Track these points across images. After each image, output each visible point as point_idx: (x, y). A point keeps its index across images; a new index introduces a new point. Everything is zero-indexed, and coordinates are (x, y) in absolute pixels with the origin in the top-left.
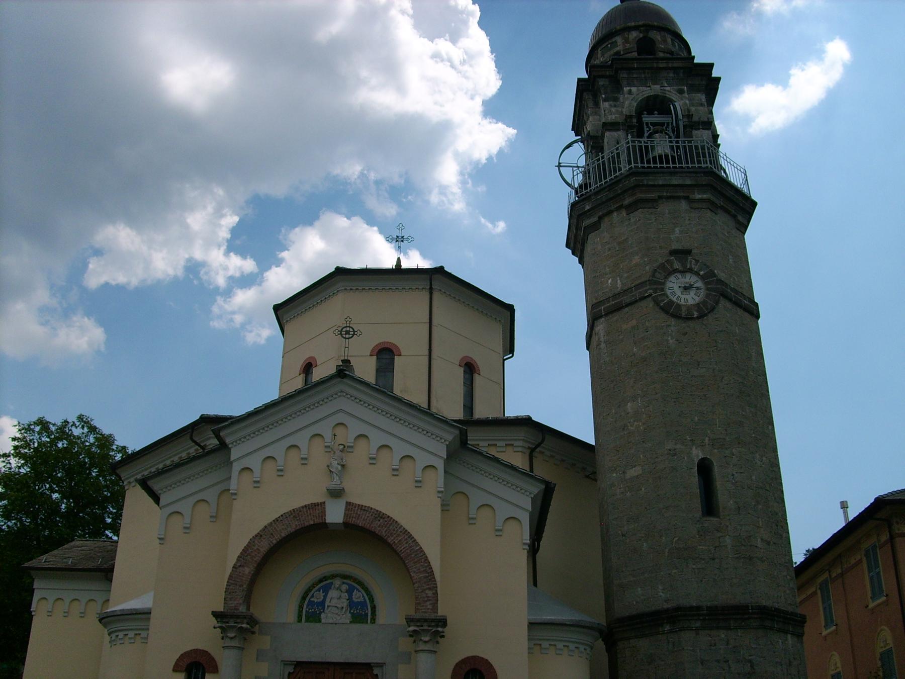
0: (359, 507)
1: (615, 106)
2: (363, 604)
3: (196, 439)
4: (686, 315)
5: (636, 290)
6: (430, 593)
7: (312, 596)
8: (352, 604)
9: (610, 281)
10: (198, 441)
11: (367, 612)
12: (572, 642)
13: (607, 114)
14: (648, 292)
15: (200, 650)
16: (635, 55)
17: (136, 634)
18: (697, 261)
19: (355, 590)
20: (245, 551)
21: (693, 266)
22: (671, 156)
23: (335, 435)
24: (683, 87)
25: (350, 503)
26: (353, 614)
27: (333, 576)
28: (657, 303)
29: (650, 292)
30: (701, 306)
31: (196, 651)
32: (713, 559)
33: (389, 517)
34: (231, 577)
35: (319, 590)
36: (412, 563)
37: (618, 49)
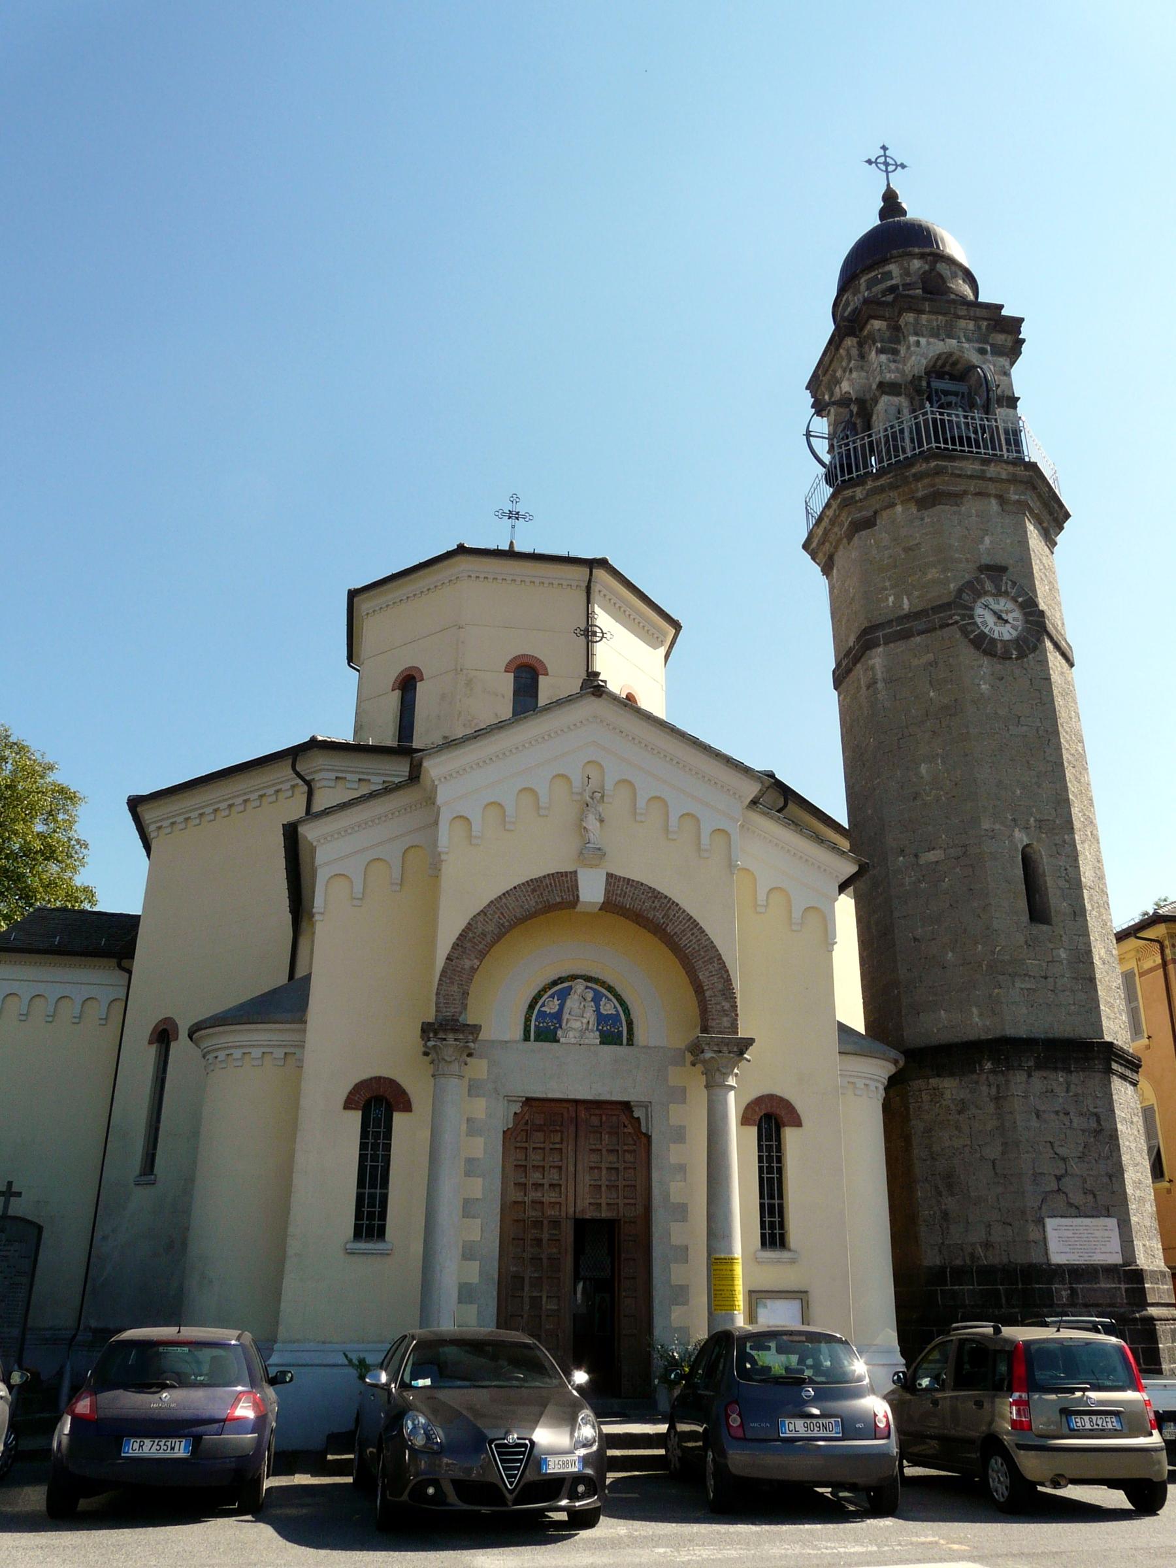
0: (624, 881)
1: (895, 361)
2: (615, 1018)
3: (298, 769)
4: (1001, 653)
5: (934, 614)
6: (727, 1006)
7: (543, 1005)
8: (601, 1018)
9: (891, 599)
10: (302, 773)
11: (621, 1029)
12: (860, 1077)
13: (885, 371)
14: (954, 618)
15: (384, 1078)
16: (919, 292)
17: (244, 1053)
18: (1014, 583)
19: (604, 999)
20: (462, 936)
21: (1009, 590)
22: (966, 437)
23: (589, 778)
24: (985, 346)
25: (612, 874)
26: (601, 1031)
27: (573, 978)
28: (965, 632)
29: (957, 618)
30: (1021, 643)
31: (378, 1080)
32: (1046, 978)
33: (666, 897)
34: (444, 973)
35: (552, 996)
36: (700, 962)
37: (893, 282)
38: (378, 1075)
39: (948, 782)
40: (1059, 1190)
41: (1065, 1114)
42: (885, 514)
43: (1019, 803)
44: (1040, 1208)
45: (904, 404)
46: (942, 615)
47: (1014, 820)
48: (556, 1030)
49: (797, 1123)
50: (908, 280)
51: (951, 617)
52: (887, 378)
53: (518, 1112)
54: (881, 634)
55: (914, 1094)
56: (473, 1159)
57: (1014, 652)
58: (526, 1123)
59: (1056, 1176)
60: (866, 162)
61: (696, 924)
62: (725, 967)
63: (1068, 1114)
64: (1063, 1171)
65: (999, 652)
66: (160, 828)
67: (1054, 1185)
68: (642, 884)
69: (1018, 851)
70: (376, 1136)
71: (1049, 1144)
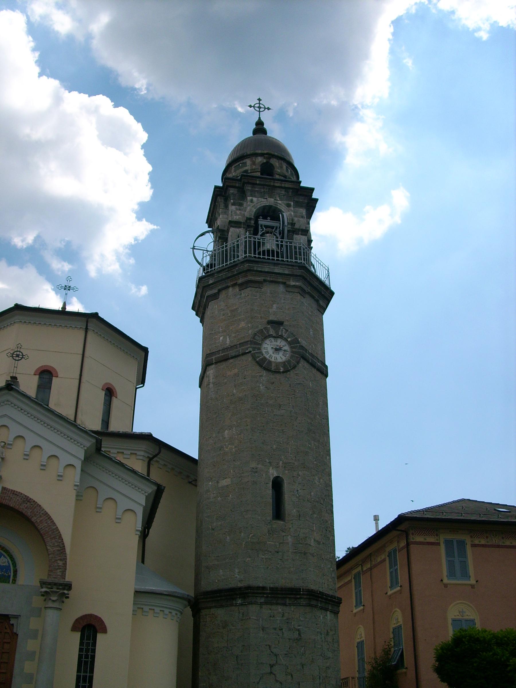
1: (240, 210)
5: (240, 347)
6: (61, 563)
9: (221, 338)
11: (10, 574)
16: (258, 174)
18: (287, 331)
22: (276, 251)
28: (254, 357)
29: (251, 349)
33: (34, 501)
40: (271, 673)
41: (280, 629)
43: (274, 453)
44: (258, 683)
45: (242, 233)
46: (243, 348)
47: (270, 462)
49: (104, 630)
50: (254, 167)
52: (234, 218)
54: (214, 358)
57: (282, 369)
59: (270, 665)
60: (270, 109)
61: (50, 518)
62: (63, 541)
63: (282, 629)
64: (275, 662)
65: (273, 368)
67: (268, 670)
68: (22, 494)
69: (270, 480)
71: (268, 647)
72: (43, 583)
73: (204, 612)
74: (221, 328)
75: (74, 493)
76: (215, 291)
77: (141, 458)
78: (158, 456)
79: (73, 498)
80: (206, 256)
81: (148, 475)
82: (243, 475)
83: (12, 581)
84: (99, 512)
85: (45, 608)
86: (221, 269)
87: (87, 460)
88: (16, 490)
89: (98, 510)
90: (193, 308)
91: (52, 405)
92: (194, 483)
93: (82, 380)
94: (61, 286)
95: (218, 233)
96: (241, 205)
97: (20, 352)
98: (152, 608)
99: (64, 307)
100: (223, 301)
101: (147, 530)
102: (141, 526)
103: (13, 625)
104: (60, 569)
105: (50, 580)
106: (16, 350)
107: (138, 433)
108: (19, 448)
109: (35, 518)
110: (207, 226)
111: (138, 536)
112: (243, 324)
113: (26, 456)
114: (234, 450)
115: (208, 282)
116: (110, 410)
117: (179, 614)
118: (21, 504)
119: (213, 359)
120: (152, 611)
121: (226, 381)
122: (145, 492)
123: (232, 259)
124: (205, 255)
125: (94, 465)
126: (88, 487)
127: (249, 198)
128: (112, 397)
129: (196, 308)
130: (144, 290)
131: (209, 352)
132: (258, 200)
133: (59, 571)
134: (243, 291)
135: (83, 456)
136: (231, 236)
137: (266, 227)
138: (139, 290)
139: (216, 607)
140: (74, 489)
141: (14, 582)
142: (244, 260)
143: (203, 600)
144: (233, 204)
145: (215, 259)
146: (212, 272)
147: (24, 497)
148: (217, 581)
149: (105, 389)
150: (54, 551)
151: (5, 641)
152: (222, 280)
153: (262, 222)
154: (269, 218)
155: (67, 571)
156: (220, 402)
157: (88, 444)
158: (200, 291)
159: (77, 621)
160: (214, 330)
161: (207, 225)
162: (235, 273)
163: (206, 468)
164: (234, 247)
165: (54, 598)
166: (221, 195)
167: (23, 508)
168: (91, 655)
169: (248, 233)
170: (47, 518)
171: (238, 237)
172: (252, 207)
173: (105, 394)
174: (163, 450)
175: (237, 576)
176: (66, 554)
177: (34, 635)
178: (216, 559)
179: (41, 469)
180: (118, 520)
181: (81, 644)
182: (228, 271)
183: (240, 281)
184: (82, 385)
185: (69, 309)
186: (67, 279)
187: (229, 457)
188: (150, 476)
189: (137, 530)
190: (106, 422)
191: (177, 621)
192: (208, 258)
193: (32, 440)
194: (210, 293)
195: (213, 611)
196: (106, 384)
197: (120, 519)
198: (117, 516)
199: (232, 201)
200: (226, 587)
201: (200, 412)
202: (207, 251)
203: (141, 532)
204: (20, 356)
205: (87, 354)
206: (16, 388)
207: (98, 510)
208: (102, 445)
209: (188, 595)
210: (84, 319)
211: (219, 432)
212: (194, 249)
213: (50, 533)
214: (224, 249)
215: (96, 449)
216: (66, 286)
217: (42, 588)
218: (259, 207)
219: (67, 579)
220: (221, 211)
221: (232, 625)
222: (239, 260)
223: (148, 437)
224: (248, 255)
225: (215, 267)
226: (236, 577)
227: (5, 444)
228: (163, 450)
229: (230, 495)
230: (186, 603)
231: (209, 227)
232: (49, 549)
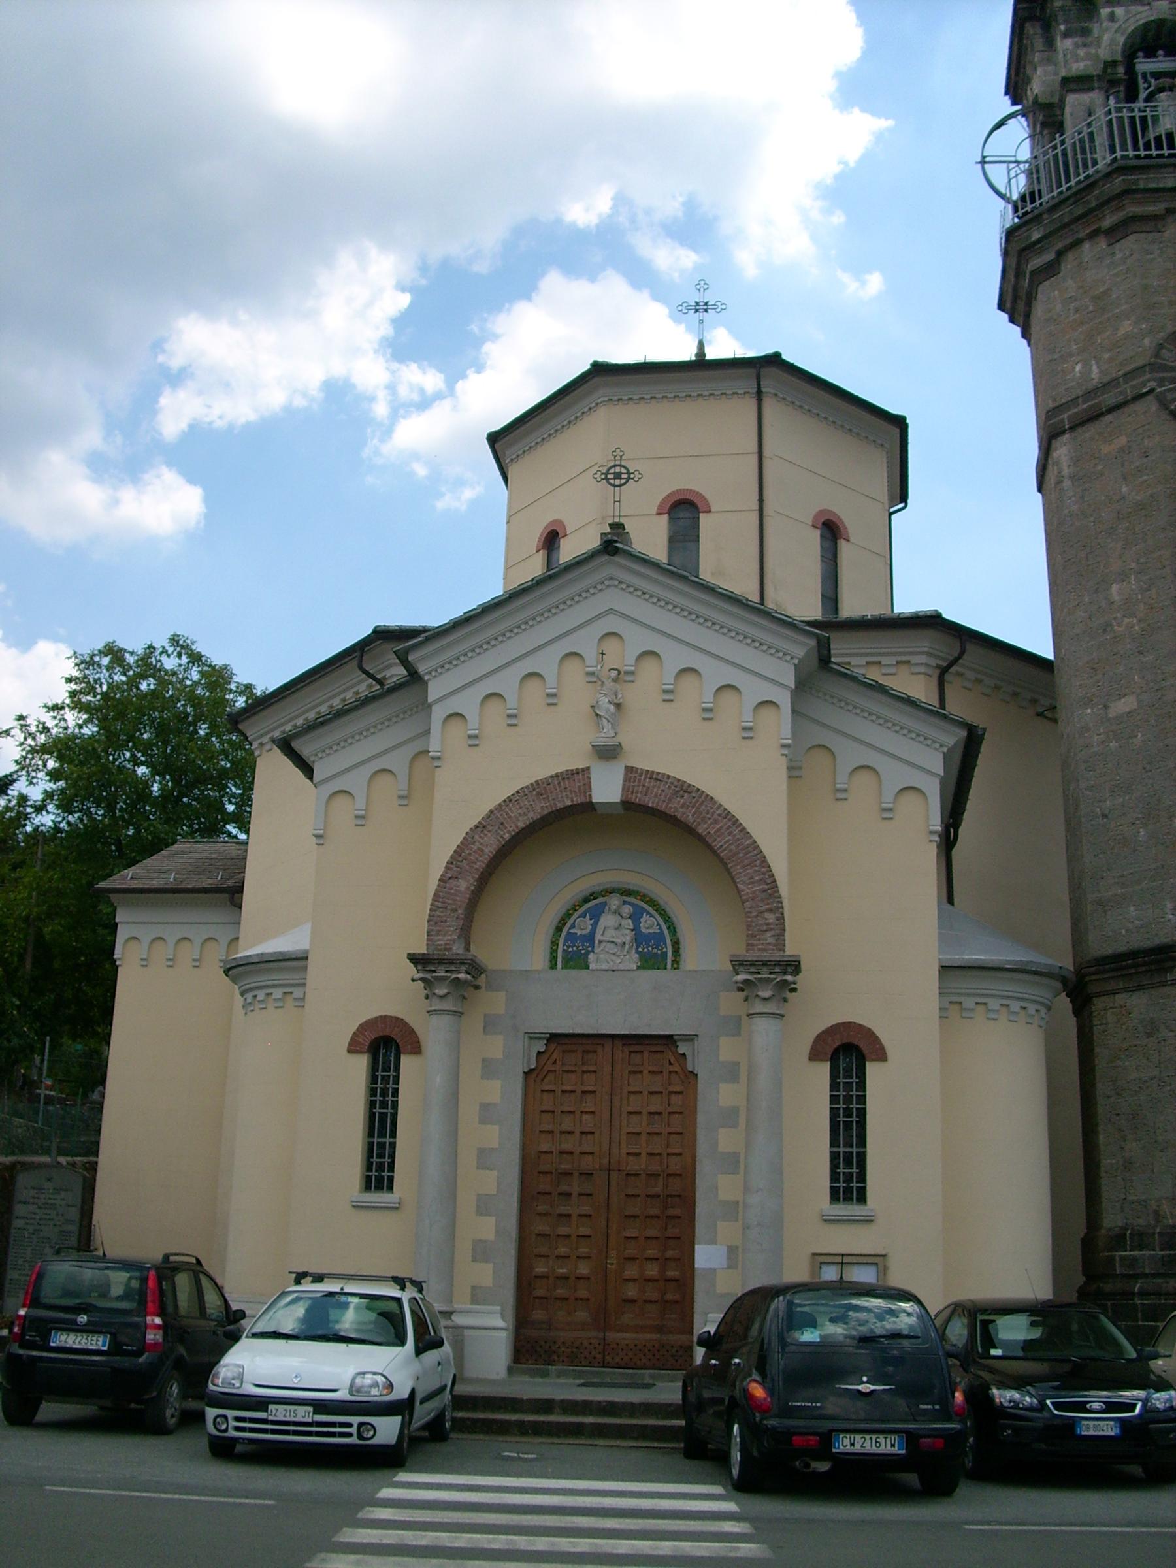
1: (1085, 45)
2: (659, 938)
6: (771, 918)
7: (573, 926)
8: (639, 938)
9: (1078, 368)
17: (285, 993)
20: (458, 852)
23: (602, 654)
29: (1152, 384)
31: (383, 1019)
33: (698, 790)
34: (436, 897)
35: (583, 915)
38: (383, 1014)
39: (1142, 605)
42: (1070, 256)
46: (1134, 382)
48: (588, 953)
49: (881, 1055)
51: (1144, 384)
53: (542, 1050)
54: (1066, 416)
55: (1099, 1014)
56: (489, 1105)
58: (555, 1062)
61: (736, 822)
66: (262, 745)
68: (669, 776)
70: (385, 1080)
72: (738, 964)
73: (1099, 1003)
74: (1073, 343)
75: (783, 763)
76: (1049, 256)
77: (923, 669)
78: (960, 661)
79: (783, 773)
80: (1016, 176)
81: (942, 705)
82: (1164, 684)
83: (672, 965)
84: (841, 799)
85: (749, 1015)
86: (1057, 200)
87: (803, 687)
88: (656, 770)
89: (840, 794)
90: (1001, 306)
91: (706, 573)
92: (1049, 714)
93: (767, 511)
94: (685, 305)
95: (1037, 112)
96: (1086, 32)
97: (620, 466)
98: (1005, 1002)
99: (701, 353)
100: (1072, 278)
101: (952, 830)
102: (939, 823)
103: (684, 1055)
104: (771, 929)
105: (752, 956)
106: (613, 464)
107: (909, 615)
108: (650, 678)
109: (705, 826)
110: (1009, 102)
111: (935, 845)
112: (1126, 327)
113: (669, 695)
114: (1137, 628)
115: (1029, 237)
116: (836, 572)
117: (1043, 1011)
118: (670, 800)
119: (1063, 419)
120: (956, 1007)
121: (1100, 467)
122: (941, 746)
123: (1081, 171)
124: (1012, 174)
125: (818, 697)
126: (814, 747)
127: (1105, 12)
128: (838, 541)
129: (1008, 305)
130: (875, 282)
131: (1051, 405)
132: (1127, 12)
133: (769, 934)
134: (1117, 246)
135: (793, 678)
136: (1071, 115)
137: (1157, 75)
138: (863, 283)
139: (1125, 990)
140: (783, 755)
141: (675, 966)
142: (1110, 169)
143: (1093, 977)
144: (1066, 35)
145: (1038, 179)
146: (1036, 212)
147: (676, 783)
148: (1124, 932)
149: (820, 525)
150: (754, 893)
151: (671, 1089)
152: (1065, 226)
153: (1144, 65)
154: (1161, 52)
155: (787, 934)
156: (1092, 519)
157: (800, 652)
158: (1013, 261)
159: (821, 1038)
160: (1057, 351)
161: (1007, 100)
162: (1094, 204)
163: (1076, 676)
164: (1081, 141)
165: (766, 994)
166: (1031, 18)
167: (675, 807)
168: (857, 1109)
169: (1112, 101)
170: (730, 823)
171: (1090, 115)
172: (1116, 32)
173: (821, 536)
174: (970, 647)
175: (1171, 916)
176: (780, 897)
177: (732, 1073)
178: (1118, 883)
179: (704, 719)
180: (887, 813)
181: (834, 1086)
182: (1074, 203)
183: (1107, 223)
184: (767, 521)
185: (711, 354)
186: (698, 287)
187: (1128, 646)
188: (947, 706)
189: (931, 832)
190: (831, 598)
191: (1040, 1027)
192: (1022, 180)
193: (675, 658)
194: (1036, 262)
195: (1120, 998)
196: (822, 512)
197: (890, 810)
198: (884, 805)
199: (1062, 27)
200: (1148, 944)
201: (1048, 550)
202: (1017, 162)
203: (940, 836)
204: (623, 476)
205: (767, 452)
206: (626, 548)
207: (840, 795)
208: (832, 652)
209: (1061, 968)
210: (753, 371)
211: (1096, 591)
212: (985, 162)
213: (741, 855)
214: (1059, 150)
215: (820, 660)
216: (697, 304)
217: (737, 974)
218: (1130, 30)
219: (790, 950)
220: (1037, 57)
221: (1167, 1027)
222: (1097, 172)
223: (932, 622)
224: (1118, 154)
225: (1040, 198)
226: (1169, 920)
227: (619, 673)
228: (970, 647)
229: (1139, 734)
230: (1058, 985)
231: (1014, 103)
232: (743, 891)
